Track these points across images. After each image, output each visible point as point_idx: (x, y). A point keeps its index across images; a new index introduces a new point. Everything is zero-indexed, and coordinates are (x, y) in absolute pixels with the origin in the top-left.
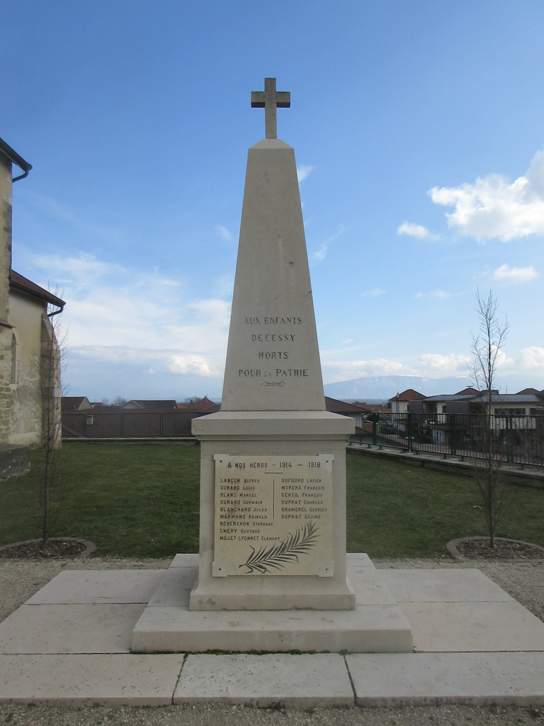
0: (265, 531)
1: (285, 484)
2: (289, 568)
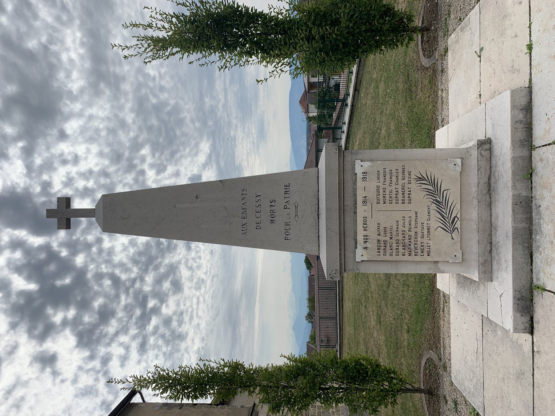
1: (382, 201)
2: (453, 197)
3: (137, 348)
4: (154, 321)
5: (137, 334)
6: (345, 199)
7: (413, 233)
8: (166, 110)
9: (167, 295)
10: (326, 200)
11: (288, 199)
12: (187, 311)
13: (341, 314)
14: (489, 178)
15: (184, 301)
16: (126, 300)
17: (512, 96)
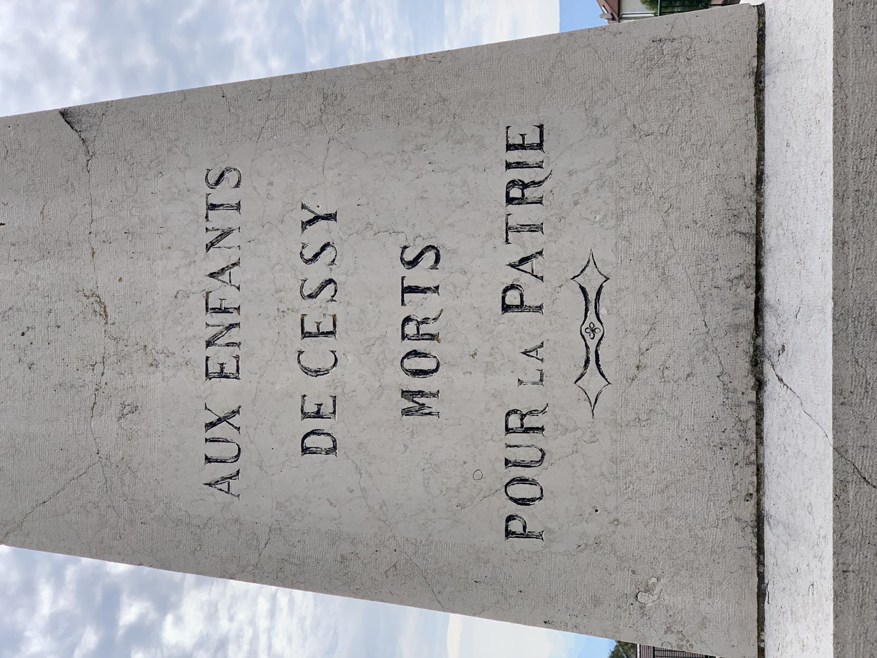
8: (180, 21)
10: (840, 243)
12: (239, 637)
15: (230, 608)
16: (55, 600)
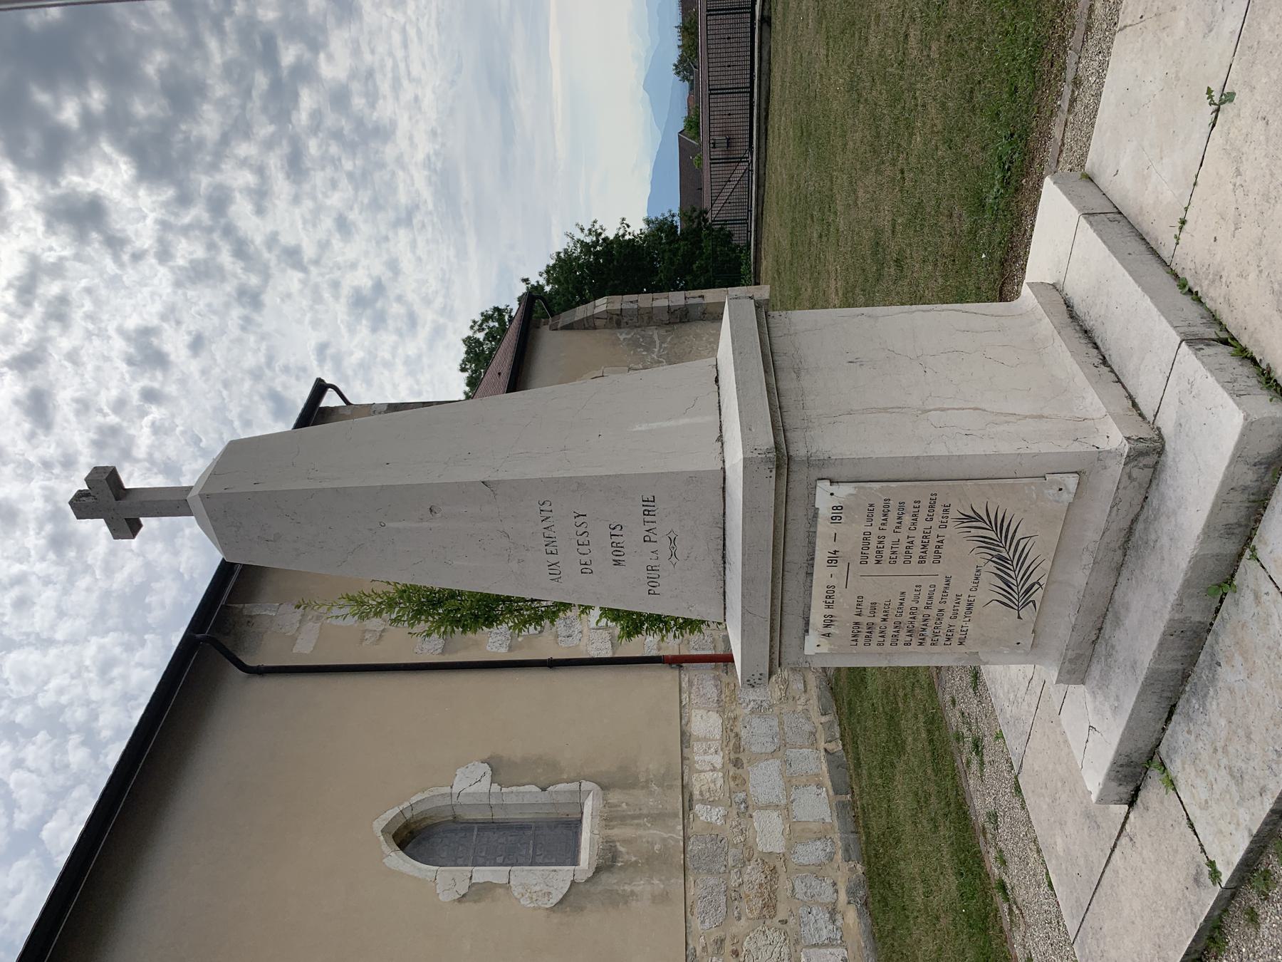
0: (961, 586)
1: (872, 560)
3: (282, 167)
4: (307, 100)
5: (273, 135)
6: (788, 550)
7: (934, 612)
9: (323, 30)
10: (743, 565)
11: (652, 526)
12: (382, 67)
13: (763, 150)
14: (1134, 521)
15: (369, 43)
16: (223, 51)
17: (1243, 435)
